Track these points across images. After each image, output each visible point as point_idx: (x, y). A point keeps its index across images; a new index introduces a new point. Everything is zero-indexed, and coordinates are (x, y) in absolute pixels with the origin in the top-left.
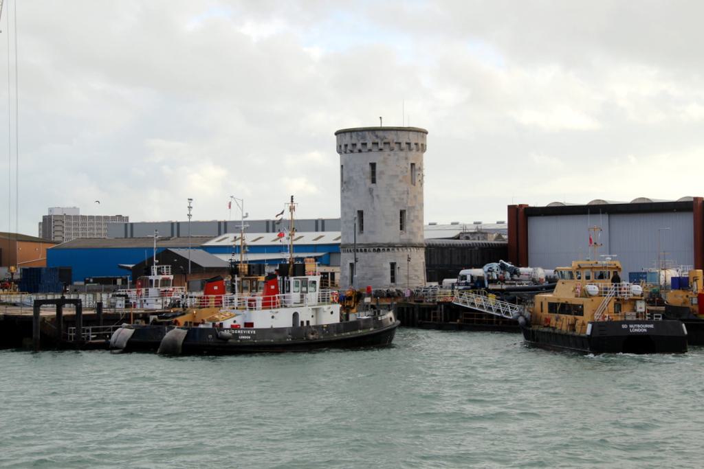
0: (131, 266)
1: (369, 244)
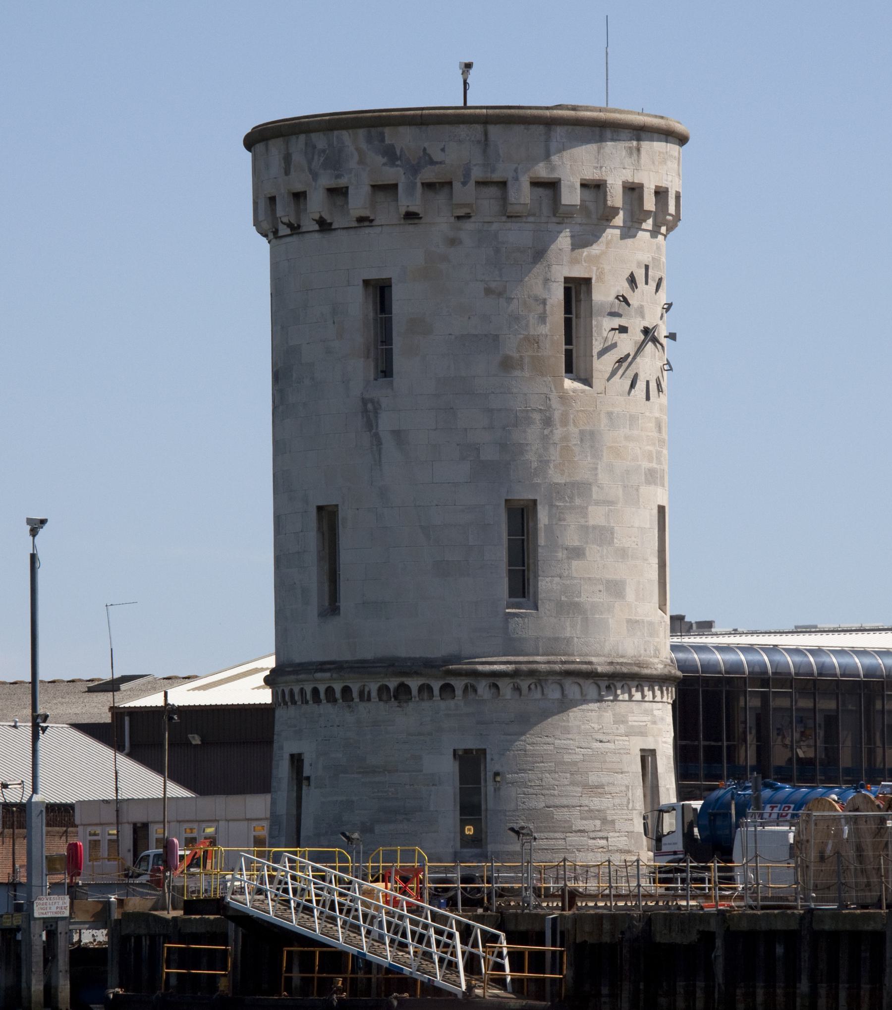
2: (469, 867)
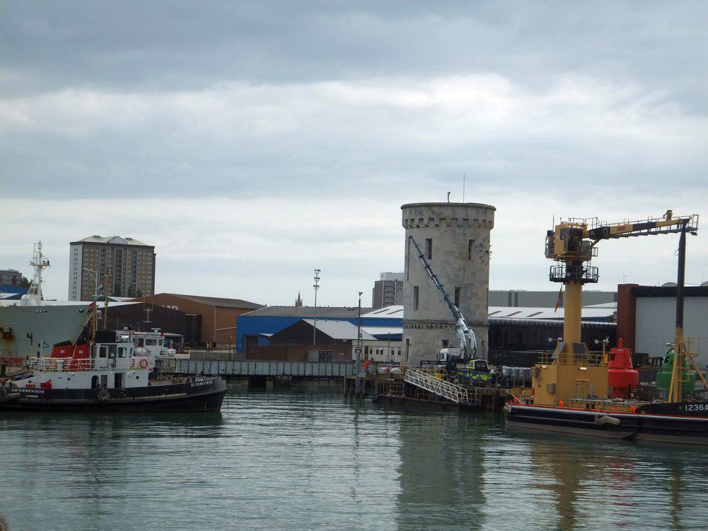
0: (270, 335)
1: (423, 321)
2: (197, 397)
